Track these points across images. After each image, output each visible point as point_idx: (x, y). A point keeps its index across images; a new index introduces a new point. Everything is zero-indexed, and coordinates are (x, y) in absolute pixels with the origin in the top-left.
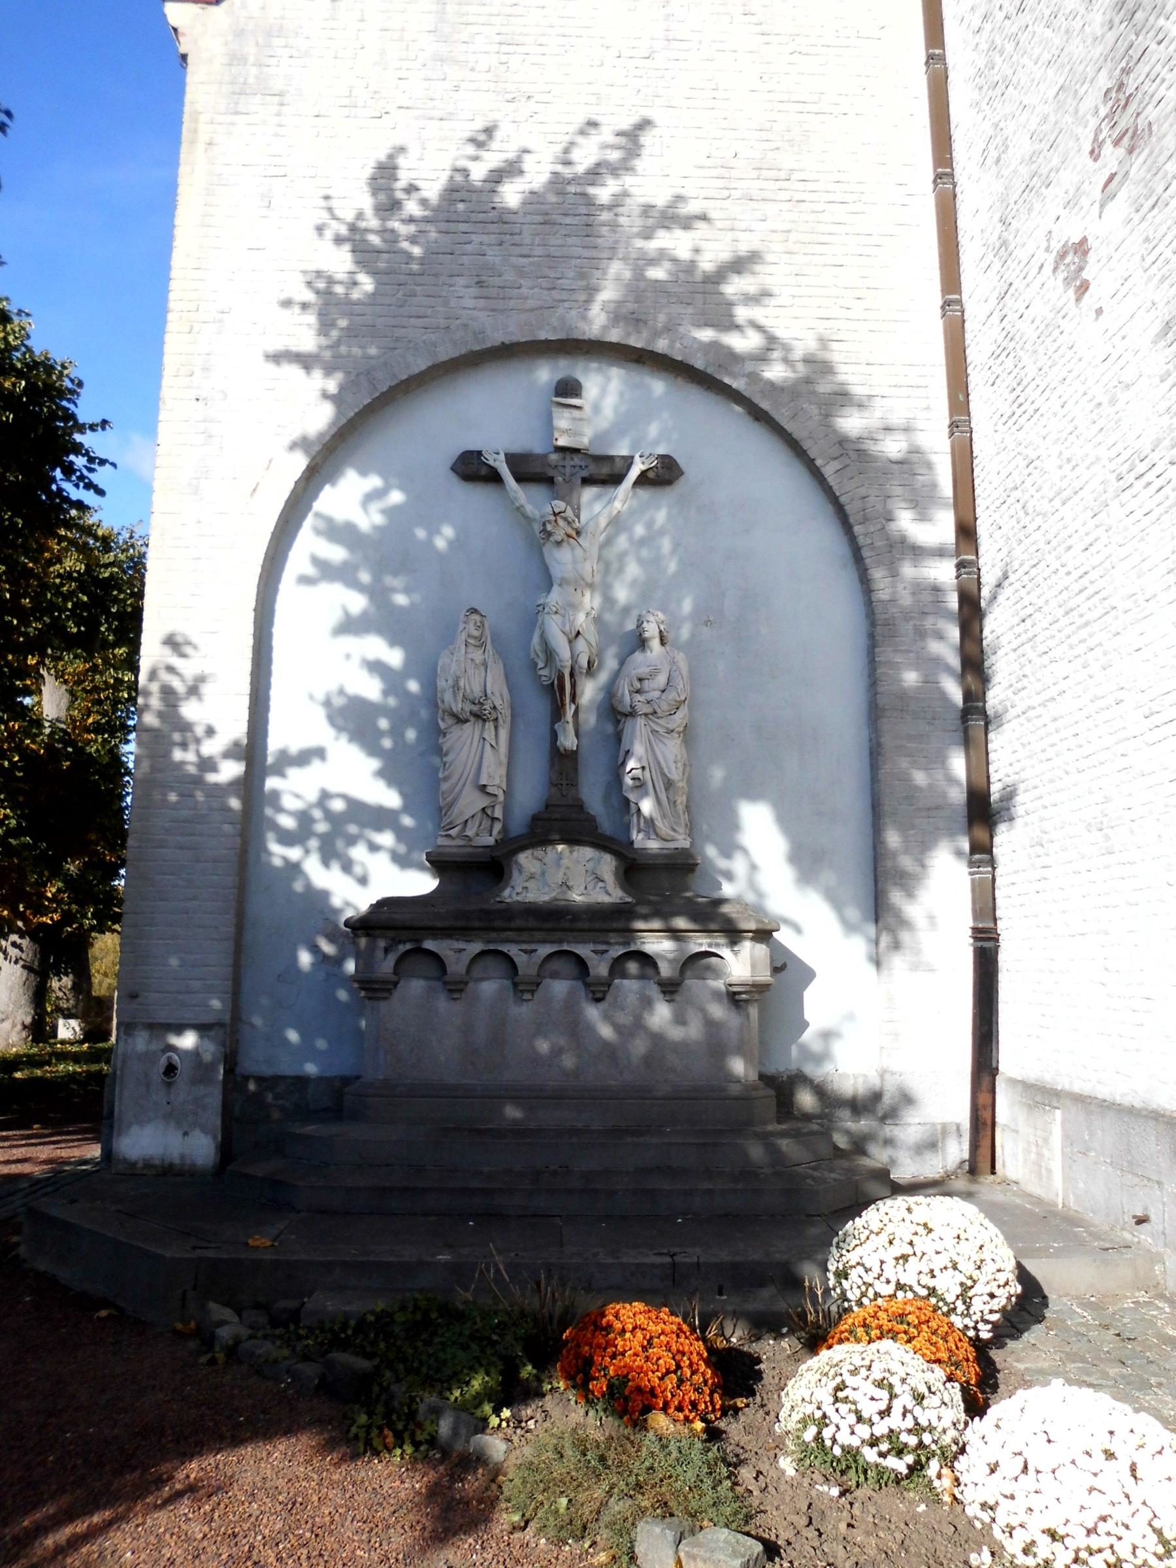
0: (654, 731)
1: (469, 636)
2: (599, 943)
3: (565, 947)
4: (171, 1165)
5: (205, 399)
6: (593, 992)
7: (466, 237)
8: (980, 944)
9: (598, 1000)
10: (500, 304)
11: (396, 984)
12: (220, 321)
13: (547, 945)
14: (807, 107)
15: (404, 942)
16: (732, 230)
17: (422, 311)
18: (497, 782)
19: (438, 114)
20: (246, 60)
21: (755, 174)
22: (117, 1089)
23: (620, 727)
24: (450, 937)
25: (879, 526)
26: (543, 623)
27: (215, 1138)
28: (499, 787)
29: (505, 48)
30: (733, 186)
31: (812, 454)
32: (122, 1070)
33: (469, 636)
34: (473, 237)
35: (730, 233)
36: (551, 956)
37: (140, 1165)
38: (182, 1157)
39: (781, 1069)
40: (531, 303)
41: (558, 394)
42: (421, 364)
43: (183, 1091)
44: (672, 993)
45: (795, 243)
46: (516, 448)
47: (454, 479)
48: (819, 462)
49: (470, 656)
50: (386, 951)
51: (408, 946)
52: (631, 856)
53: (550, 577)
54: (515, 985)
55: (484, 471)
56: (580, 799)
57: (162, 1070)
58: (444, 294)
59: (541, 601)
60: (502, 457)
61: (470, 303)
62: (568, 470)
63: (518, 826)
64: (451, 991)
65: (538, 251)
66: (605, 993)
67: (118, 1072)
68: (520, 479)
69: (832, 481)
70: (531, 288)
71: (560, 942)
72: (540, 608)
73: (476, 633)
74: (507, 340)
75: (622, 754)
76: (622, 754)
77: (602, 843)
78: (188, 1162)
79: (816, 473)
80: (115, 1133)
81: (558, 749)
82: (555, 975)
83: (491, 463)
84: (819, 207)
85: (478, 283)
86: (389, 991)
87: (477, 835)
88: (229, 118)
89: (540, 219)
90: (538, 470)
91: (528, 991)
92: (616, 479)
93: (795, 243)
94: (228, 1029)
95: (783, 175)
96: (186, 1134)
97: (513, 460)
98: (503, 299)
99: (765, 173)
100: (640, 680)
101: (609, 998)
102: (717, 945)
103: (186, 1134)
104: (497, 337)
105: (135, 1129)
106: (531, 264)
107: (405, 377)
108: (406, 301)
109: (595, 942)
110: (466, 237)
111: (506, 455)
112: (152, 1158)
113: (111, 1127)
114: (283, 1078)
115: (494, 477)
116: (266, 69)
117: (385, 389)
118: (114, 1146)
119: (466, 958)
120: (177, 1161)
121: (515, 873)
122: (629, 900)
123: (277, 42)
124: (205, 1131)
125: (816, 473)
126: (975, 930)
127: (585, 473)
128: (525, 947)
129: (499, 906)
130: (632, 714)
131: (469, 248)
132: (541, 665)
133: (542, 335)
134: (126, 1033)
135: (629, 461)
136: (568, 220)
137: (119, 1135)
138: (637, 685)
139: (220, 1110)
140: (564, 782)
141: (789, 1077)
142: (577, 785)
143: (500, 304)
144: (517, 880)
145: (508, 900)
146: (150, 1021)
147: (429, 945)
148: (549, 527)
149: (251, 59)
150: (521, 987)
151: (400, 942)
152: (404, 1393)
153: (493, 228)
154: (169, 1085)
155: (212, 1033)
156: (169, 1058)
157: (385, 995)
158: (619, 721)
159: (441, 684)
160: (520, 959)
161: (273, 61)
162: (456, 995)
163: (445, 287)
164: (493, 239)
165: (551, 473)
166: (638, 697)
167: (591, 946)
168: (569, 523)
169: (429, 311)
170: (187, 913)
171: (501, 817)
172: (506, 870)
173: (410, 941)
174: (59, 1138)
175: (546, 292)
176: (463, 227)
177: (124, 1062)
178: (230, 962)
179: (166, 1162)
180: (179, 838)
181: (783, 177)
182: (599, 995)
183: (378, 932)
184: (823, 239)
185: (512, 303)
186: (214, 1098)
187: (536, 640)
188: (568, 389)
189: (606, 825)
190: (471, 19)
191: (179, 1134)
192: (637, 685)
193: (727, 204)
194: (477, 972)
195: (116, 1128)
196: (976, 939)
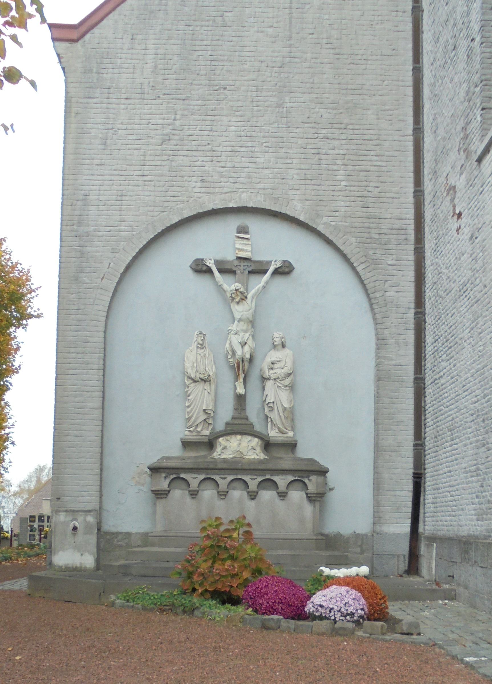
0: (278, 386)
1: (198, 344)
2: (253, 475)
3: (239, 477)
4: (76, 567)
5: (79, 236)
6: (250, 496)
7: (196, 158)
8: (415, 479)
9: (253, 499)
10: (211, 190)
11: (169, 491)
12: (85, 200)
13: (232, 476)
14: (356, 92)
15: (173, 474)
16: (319, 154)
17: (176, 194)
18: (211, 408)
19: (183, 97)
20: (92, 70)
21: (330, 126)
22: (53, 537)
23: (264, 384)
24: (192, 472)
25: (381, 295)
26: (230, 338)
27: (94, 557)
28: (211, 410)
29: (213, 63)
30: (319, 132)
31: (352, 260)
32: (55, 529)
33: (198, 344)
34: (199, 158)
35: (317, 156)
36: (233, 480)
37: (63, 567)
38: (81, 564)
39: (331, 532)
40: (226, 190)
41: (238, 232)
42: (176, 219)
43: (80, 536)
44: (284, 496)
45: (348, 160)
46: (219, 257)
47: (190, 272)
48: (355, 265)
49: (199, 352)
50: (165, 478)
51: (174, 476)
52: (267, 439)
53: (233, 317)
54: (218, 492)
55: (204, 268)
56: (247, 416)
57: (72, 529)
58: (186, 185)
59: (229, 328)
60: (212, 261)
61: (197, 190)
62: (242, 268)
63: (220, 426)
64: (191, 495)
65: (229, 164)
66: (255, 496)
67: (53, 530)
68: (220, 271)
69: (361, 273)
70: (226, 182)
71: (237, 474)
72: (230, 331)
73: (201, 342)
74: (215, 207)
75: (265, 396)
76: (265, 396)
77: (255, 435)
78: (83, 566)
79: (354, 269)
80: (53, 554)
81: (237, 393)
82: (234, 489)
83: (208, 264)
84: (360, 142)
85: (201, 180)
86: (167, 494)
87: (202, 430)
88: (85, 100)
89: (230, 149)
90: (229, 267)
91: (223, 495)
92: (265, 272)
93: (348, 160)
94: (98, 512)
95: (343, 126)
96: (82, 555)
97: (217, 263)
98: (213, 188)
99: (335, 126)
100: (273, 364)
101: (257, 498)
102: (303, 477)
103: (82, 555)
104: (210, 207)
105: (61, 553)
106: (226, 171)
107: (169, 225)
108: (169, 189)
109: (251, 475)
110: (196, 158)
111: (214, 261)
112: (68, 564)
113: (51, 552)
114: (121, 533)
115: (209, 271)
116: (101, 75)
117: (160, 231)
118: (53, 558)
119: (198, 481)
120: (78, 565)
121: (218, 446)
122: (266, 457)
123: (105, 61)
124: (90, 554)
125: (354, 269)
126: (414, 473)
127: (250, 269)
128: (222, 476)
129: (213, 460)
130: (269, 379)
131: (197, 163)
132: (229, 357)
133: (231, 205)
134: (56, 513)
135: (269, 263)
136: (243, 149)
137: (55, 554)
138: (272, 366)
139: (96, 545)
140: (240, 408)
141: (334, 535)
142: (245, 409)
143: (211, 190)
144: (219, 449)
145: (216, 457)
146: (65, 509)
147: (183, 475)
148: (233, 296)
149: (95, 70)
150: (220, 493)
151: (171, 474)
152: (246, 64)
153: (208, 154)
154: (74, 535)
155: (92, 514)
156: (74, 524)
157: (165, 496)
158: (263, 382)
159: (187, 364)
160: (220, 481)
161: (105, 71)
162: (194, 496)
163: (187, 183)
164: (208, 159)
165: (234, 269)
166: (271, 371)
167: (250, 476)
168: (242, 293)
169: (179, 194)
170: (79, 464)
171: (212, 423)
172: (214, 445)
173: (175, 474)
174: (197, 411)
175: (232, 184)
176: (194, 153)
177: (55, 526)
178: (99, 484)
179: (75, 566)
180: (75, 432)
181: (343, 128)
182: (253, 497)
183: (162, 470)
184: (366, 153)
185: (217, 190)
186: (93, 539)
187: (227, 345)
188: (243, 230)
189: (258, 427)
190: (197, 48)
191: (80, 554)
192: (272, 366)
193: (316, 141)
194: (202, 486)
195: (53, 552)
196: (414, 477)
